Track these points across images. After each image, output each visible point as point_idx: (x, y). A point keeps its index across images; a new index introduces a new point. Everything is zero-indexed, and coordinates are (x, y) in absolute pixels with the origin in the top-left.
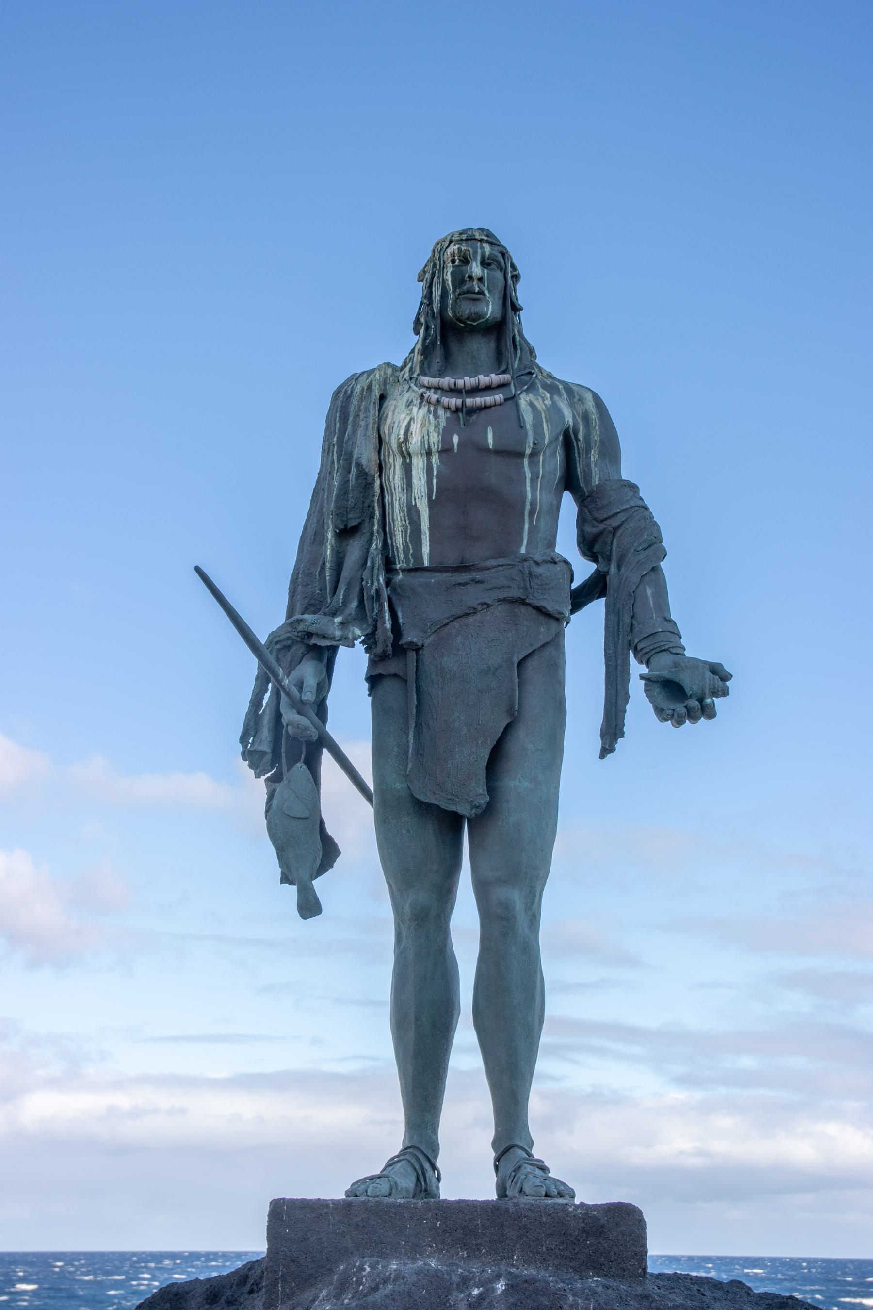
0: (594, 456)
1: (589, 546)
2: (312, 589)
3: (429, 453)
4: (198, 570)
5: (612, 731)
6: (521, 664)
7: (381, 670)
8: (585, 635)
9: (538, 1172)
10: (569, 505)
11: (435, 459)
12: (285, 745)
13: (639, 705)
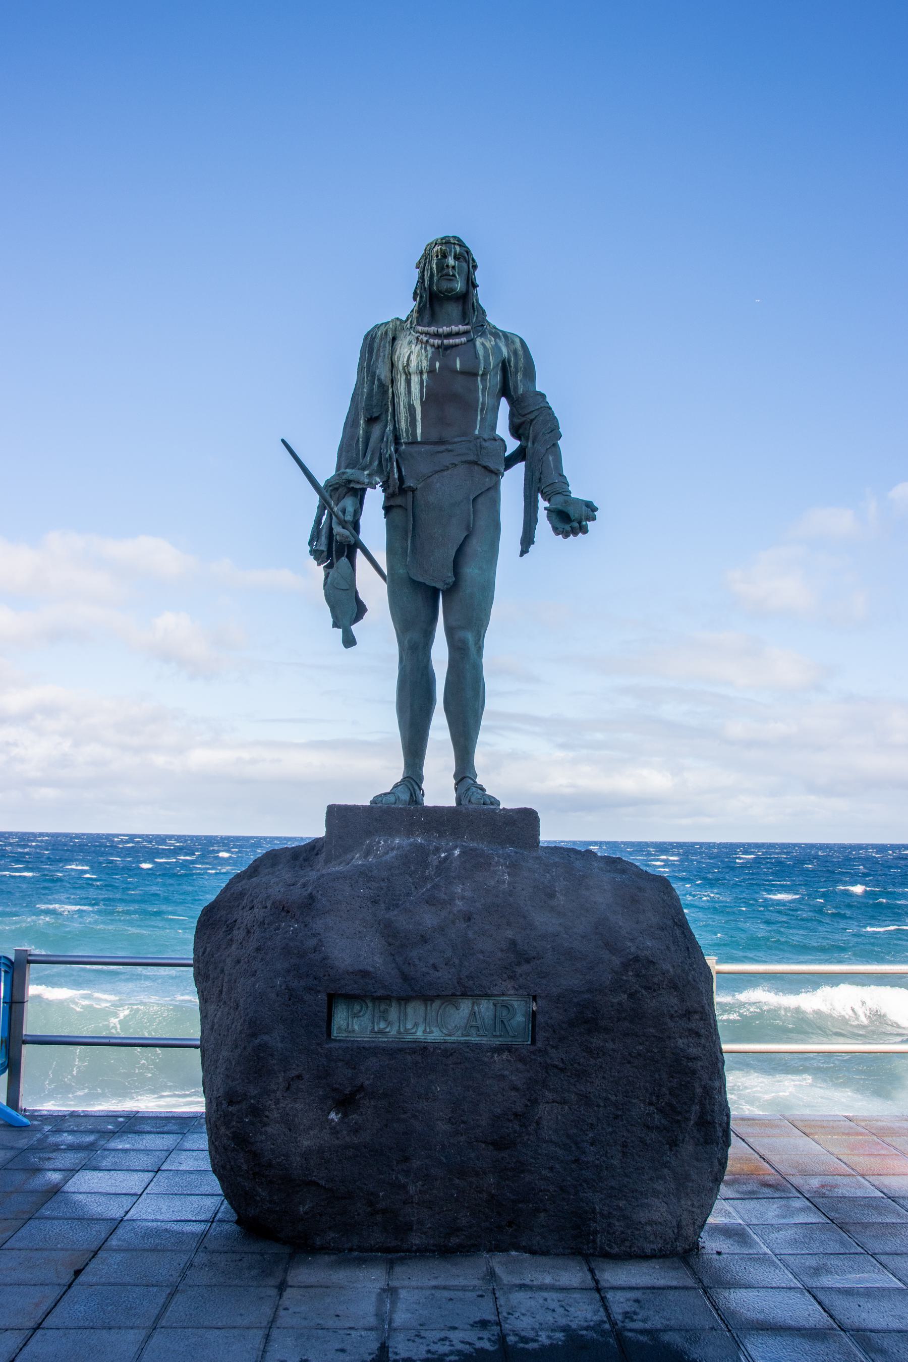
0: (520, 376)
1: (516, 430)
2: (351, 451)
3: (421, 373)
4: (283, 441)
5: (527, 540)
6: (474, 500)
7: (392, 503)
8: (512, 483)
9: (479, 791)
10: (504, 407)
11: (425, 377)
12: (336, 547)
13: (543, 525)
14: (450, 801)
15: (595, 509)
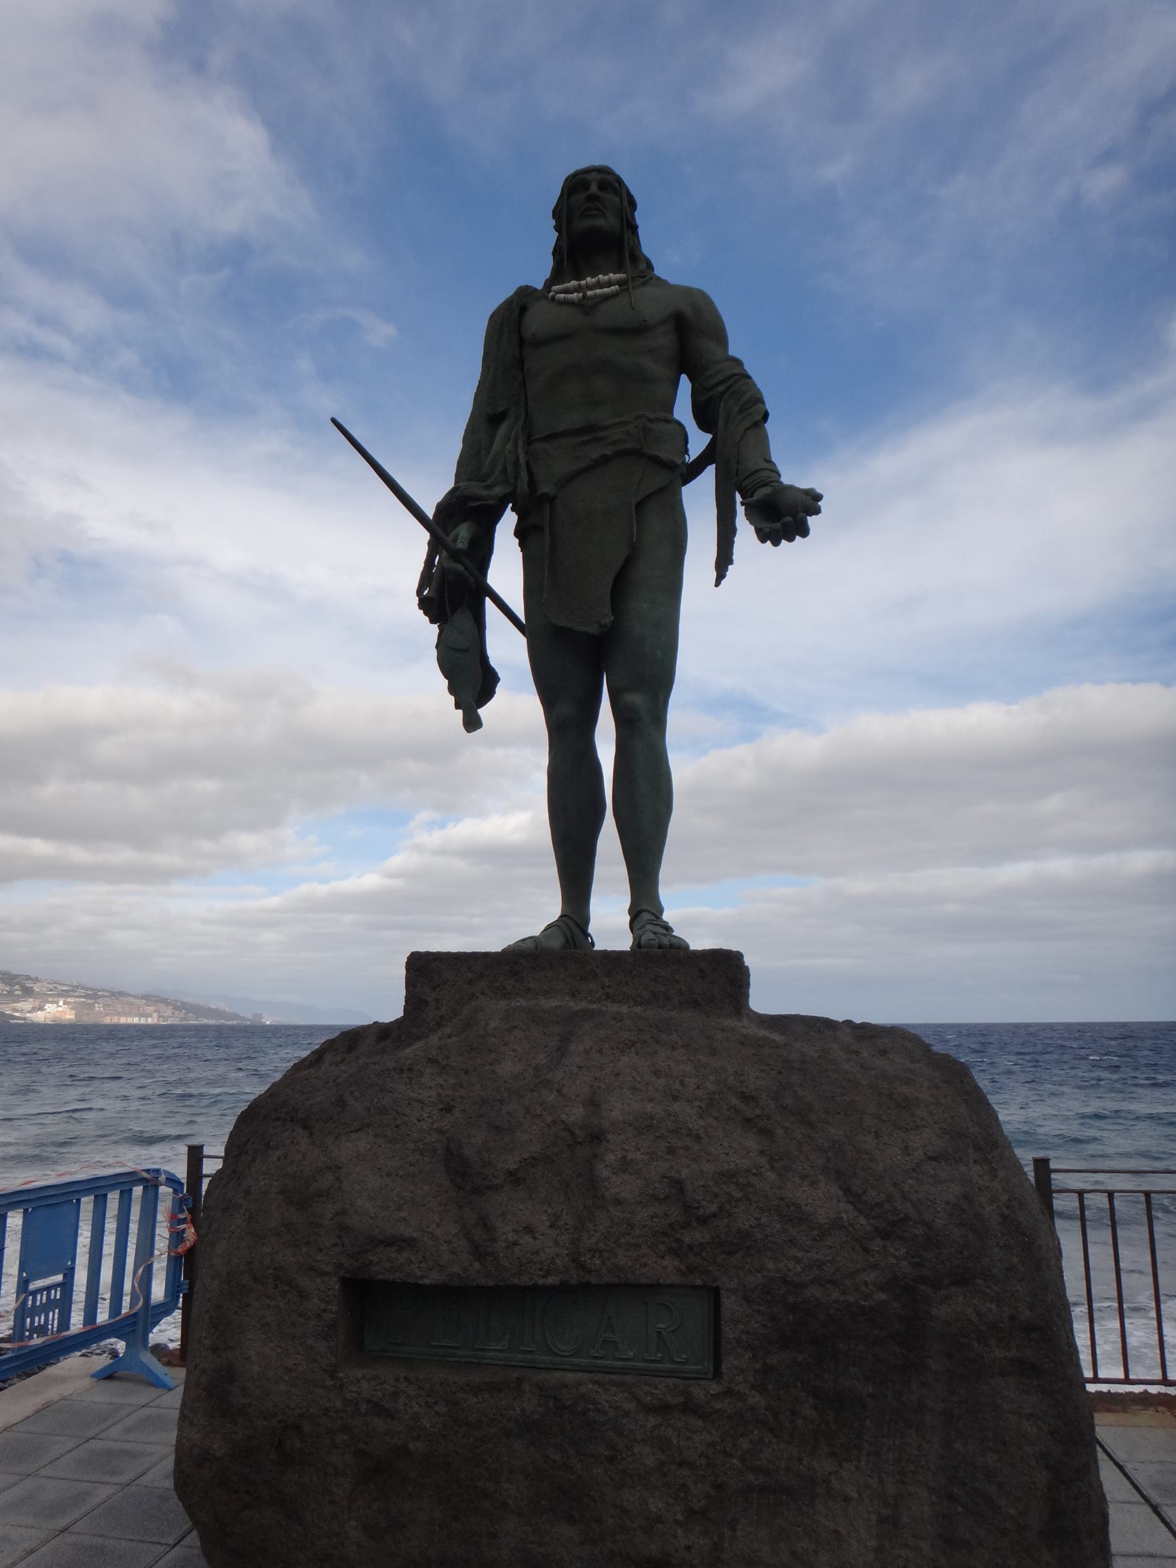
1: (704, 419)
4: (334, 421)
5: (724, 561)
6: (639, 506)
9: (664, 931)
10: (685, 385)
12: (453, 594)
13: (745, 531)
14: (624, 943)
15: (819, 497)
